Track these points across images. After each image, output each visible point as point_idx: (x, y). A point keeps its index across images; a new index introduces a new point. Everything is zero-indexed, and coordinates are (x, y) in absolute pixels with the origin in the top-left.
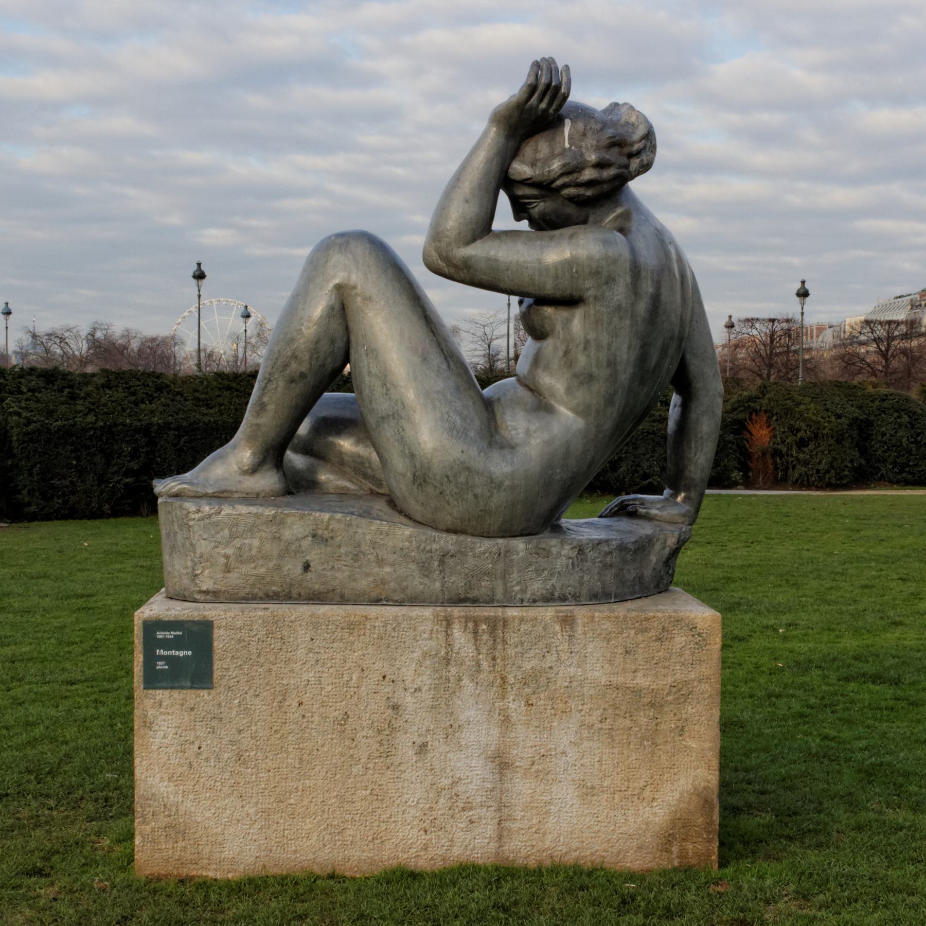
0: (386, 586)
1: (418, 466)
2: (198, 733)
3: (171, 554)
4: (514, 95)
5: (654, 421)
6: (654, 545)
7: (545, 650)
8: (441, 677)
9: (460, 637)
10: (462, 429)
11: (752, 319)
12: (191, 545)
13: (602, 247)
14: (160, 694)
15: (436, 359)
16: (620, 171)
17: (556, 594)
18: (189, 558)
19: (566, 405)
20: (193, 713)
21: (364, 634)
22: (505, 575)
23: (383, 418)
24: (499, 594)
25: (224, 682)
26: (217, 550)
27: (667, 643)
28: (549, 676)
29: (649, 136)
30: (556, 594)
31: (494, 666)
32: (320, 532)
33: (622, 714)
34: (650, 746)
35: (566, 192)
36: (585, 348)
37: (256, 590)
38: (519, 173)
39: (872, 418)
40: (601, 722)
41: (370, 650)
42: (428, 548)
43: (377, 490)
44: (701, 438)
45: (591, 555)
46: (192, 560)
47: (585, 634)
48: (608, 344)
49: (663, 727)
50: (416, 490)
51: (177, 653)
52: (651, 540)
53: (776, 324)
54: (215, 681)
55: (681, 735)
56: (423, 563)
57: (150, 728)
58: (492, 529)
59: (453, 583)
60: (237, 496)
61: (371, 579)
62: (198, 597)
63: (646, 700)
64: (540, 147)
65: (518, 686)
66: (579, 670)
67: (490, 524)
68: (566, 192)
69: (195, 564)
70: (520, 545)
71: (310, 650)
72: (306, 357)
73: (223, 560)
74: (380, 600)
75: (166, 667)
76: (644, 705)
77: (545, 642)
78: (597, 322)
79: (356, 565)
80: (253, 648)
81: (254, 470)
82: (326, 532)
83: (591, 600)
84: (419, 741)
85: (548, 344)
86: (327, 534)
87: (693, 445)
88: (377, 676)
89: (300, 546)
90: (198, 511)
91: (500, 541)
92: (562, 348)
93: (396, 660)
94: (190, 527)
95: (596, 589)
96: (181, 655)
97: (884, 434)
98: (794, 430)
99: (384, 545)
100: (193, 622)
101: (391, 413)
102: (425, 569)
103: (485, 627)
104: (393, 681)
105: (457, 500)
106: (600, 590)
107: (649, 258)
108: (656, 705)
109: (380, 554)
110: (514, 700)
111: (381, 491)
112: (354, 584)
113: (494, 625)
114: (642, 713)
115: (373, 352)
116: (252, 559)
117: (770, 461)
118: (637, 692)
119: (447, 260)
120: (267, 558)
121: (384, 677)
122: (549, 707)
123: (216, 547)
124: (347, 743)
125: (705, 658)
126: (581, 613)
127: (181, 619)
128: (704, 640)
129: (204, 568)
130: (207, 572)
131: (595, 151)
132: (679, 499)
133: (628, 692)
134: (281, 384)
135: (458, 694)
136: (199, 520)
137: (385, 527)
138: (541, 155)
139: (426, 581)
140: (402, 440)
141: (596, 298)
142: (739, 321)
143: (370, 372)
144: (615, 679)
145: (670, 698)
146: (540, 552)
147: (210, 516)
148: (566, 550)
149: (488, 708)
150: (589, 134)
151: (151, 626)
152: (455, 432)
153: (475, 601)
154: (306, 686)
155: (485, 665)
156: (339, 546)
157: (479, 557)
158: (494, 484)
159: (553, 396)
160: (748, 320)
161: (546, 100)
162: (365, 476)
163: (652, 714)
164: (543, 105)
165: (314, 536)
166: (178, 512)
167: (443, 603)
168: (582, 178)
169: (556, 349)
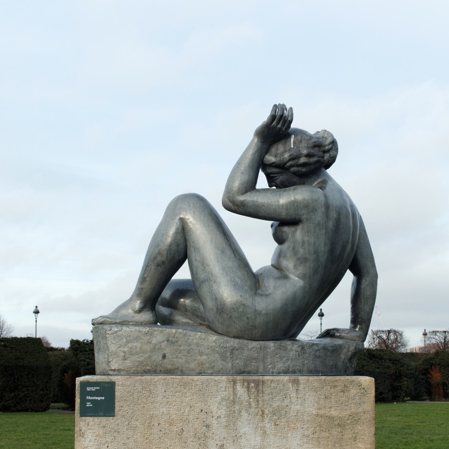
0: (204, 366)
2: (107, 439)
3: (98, 353)
4: (265, 122)
5: (385, 368)
6: (343, 350)
7: (284, 397)
8: (231, 411)
9: (241, 390)
10: (241, 285)
11: (436, 331)
13: (309, 193)
14: (89, 419)
15: (229, 252)
17: (290, 370)
19: (294, 274)
20: (104, 429)
21: (192, 389)
22: (264, 358)
23: (202, 282)
24: (261, 370)
25: (120, 413)
26: (120, 349)
27: (347, 393)
28: (286, 410)
29: (334, 143)
30: (290, 370)
31: (258, 405)
32: (170, 339)
33: (324, 430)
34: (339, 447)
35: (293, 169)
36: (303, 245)
37: (139, 369)
38: (269, 161)
40: (313, 434)
41: (195, 397)
42: (225, 346)
43: (203, 323)
45: (308, 351)
46: (108, 354)
47: (304, 388)
48: (314, 243)
49: (345, 436)
50: (218, 316)
51: (97, 398)
53: (447, 333)
54: (116, 412)
55: (355, 441)
56: (222, 353)
57: (83, 437)
59: (237, 364)
60: (131, 323)
61: (196, 362)
62: (111, 373)
63: (336, 423)
64: (280, 148)
65: (270, 415)
66: (302, 407)
67: (255, 334)
68: (293, 169)
69: (109, 356)
70: (271, 344)
71: (164, 397)
72: (165, 253)
73: (122, 354)
74: (201, 373)
75: (91, 405)
76: (335, 425)
77: (284, 393)
78: (308, 232)
79: (188, 355)
80: (135, 396)
81: (140, 311)
82: (173, 339)
83: (308, 373)
84: (220, 443)
85: (285, 246)
86: (174, 340)
87: (363, 301)
88: (198, 410)
90: (111, 330)
91: (261, 342)
92: (292, 246)
93: (208, 402)
94: (107, 337)
95: (311, 368)
96: (99, 399)
99: (203, 345)
100: (105, 382)
101: (206, 279)
102: (223, 357)
103: (253, 385)
104: (206, 413)
106: (313, 369)
107: (335, 201)
108: (341, 425)
109: (201, 349)
110: (268, 423)
112: (188, 365)
113: (257, 383)
114: (334, 430)
115: (197, 249)
116: (137, 353)
117: (441, 388)
118: (332, 418)
119: (233, 202)
120: (144, 352)
121: (202, 411)
122: (286, 426)
123: (120, 347)
124: (182, 445)
125: (366, 401)
126: (302, 379)
127: (99, 381)
128: (366, 391)
130: (114, 360)
131: (306, 149)
132: (357, 329)
133: (327, 418)
135: (239, 419)
136: (111, 334)
137: (203, 335)
138: (279, 152)
139: (223, 363)
140: (211, 292)
142: (429, 332)
143: (196, 259)
144: (322, 412)
145: (349, 422)
146: (282, 348)
147: (116, 332)
149: (255, 427)
150: (303, 141)
151: (84, 385)
152: (237, 287)
153: (249, 373)
154: (162, 415)
155: (253, 404)
156: (180, 346)
157: (250, 350)
158: (257, 313)
159: (288, 270)
160: (433, 332)
161: (281, 123)
162: (197, 316)
163: (339, 430)
164: (279, 126)
165: (168, 341)
167: (232, 374)
168: (300, 162)
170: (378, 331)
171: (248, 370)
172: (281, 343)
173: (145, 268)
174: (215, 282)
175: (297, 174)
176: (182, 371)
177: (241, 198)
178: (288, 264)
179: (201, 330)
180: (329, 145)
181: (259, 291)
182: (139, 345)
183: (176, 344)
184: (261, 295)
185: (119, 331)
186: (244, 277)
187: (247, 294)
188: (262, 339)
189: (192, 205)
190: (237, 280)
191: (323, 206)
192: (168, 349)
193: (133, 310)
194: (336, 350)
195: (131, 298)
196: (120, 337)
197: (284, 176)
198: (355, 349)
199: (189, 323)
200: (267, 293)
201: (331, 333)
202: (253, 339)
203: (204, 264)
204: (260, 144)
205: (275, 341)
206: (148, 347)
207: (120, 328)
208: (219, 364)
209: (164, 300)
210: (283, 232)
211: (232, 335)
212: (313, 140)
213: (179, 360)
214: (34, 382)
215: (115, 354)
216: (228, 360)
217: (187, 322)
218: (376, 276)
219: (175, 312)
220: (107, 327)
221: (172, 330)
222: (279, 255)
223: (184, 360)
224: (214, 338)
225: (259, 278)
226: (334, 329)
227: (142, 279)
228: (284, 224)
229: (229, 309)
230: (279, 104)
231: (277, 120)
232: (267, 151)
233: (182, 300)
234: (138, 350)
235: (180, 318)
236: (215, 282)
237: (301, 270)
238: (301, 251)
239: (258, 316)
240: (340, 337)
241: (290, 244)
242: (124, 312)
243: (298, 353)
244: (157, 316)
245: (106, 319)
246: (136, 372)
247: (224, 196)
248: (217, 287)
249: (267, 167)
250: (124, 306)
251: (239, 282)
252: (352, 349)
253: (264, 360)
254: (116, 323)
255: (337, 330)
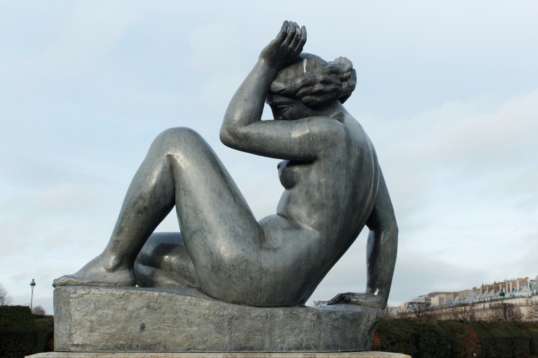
1: (215, 259)
3: (58, 322)
4: (273, 40)
10: (243, 236)
12: (70, 314)
13: (327, 125)
15: (227, 196)
16: (336, 87)
17: (304, 345)
18: (68, 323)
19: (307, 223)
22: (271, 332)
23: (194, 232)
24: (267, 345)
26: (85, 317)
29: (352, 70)
30: (304, 345)
32: (152, 304)
35: (305, 98)
36: (319, 188)
37: (110, 344)
38: (278, 87)
39: (420, 334)
44: (387, 255)
45: (325, 320)
46: (70, 325)
48: (333, 185)
52: (360, 315)
58: (262, 301)
59: (237, 337)
60: (102, 285)
61: (184, 335)
62: (73, 349)
64: (291, 72)
67: (260, 298)
68: (305, 98)
69: (71, 327)
70: (280, 312)
72: (148, 196)
74: (190, 349)
79: (174, 325)
81: (115, 269)
82: (156, 304)
83: (326, 349)
85: (295, 191)
86: (156, 306)
87: (382, 260)
89: (139, 314)
90: (75, 293)
91: (267, 309)
92: (305, 189)
94: (69, 302)
97: (425, 340)
98: (389, 338)
101: (198, 228)
102: (219, 329)
105: (239, 281)
109: (190, 318)
111: (195, 285)
112: (173, 338)
115: (188, 193)
116: (108, 323)
119: (234, 135)
123: (86, 315)
129: (77, 330)
130: (78, 332)
134: (133, 215)
136: (75, 298)
137: (194, 300)
138: (290, 77)
139: (219, 336)
141: (325, 156)
143: (186, 205)
147: (83, 295)
148: (310, 315)
150: (318, 66)
152: (238, 238)
153: (251, 349)
156: (164, 314)
158: (263, 271)
159: (299, 219)
162: (185, 277)
164: (291, 46)
165: (148, 307)
166: (63, 294)
167: (230, 350)
168: (314, 89)
169: (301, 191)
170: (319, 302)
171: (251, 345)
172: (293, 310)
173: (122, 216)
174: (210, 232)
175: (311, 104)
176: (165, 347)
177: (243, 130)
178: (301, 211)
179: (191, 293)
180: (348, 72)
181: (265, 245)
182: (111, 312)
183: (158, 311)
184: (268, 249)
185: (86, 294)
186: (247, 226)
187: (251, 248)
188: (268, 305)
189: (183, 140)
190: (238, 229)
191: (344, 140)
192: (148, 318)
193: (105, 268)
194: (355, 319)
195: (103, 253)
196: (87, 301)
197: (294, 107)
198: (377, 318)
199: (175, 285)
200: (275, 247)
201: (346, 298)
202: (257, 305)
203: (196, 210)
204: (267, 67)
205: (284, 308)
206: (122, 315)
207: (87, 290)
208: (214, 338)
209: (144, 257)
210: (293, 173)
211: (231, 300)
212: (328, 66)
213: (162, 333)
214: (20, 347)
215: (79, 324)
216: (226, 332)
217: (173, 284)
218: (396, 230)
219: (158, 272)
220: (70, 289)
221: (154, 293)
222: (288, 201)
223: (168, 332)
224: (208, 304)
225: (264, 229)
226: (349, 294)
227: (119, 230)
228: (294, 162)
229: (228, 267)
230: (291, 22)
231: (288, 39)
232: (275, 77)
233: (167, 257)
234: (109, 318)
235: (163, 279)
236: (210, 232)
237: (315, 219)
238: (317, 195)
239: (264, 275)
240: (357, 303)
241: (302, 188)
242: (94, 270)
243: (313, 323)
244: (135, 276)
245: (70, 279)
246: (105, 347)
247: (223, 127)
248: (212, 239)
249: (274, 96)
250: (94, 263)
251: (241, 232)
252: (373, 317)
253: (271, 333)
254: (82, 284)
255: (353, 295)
